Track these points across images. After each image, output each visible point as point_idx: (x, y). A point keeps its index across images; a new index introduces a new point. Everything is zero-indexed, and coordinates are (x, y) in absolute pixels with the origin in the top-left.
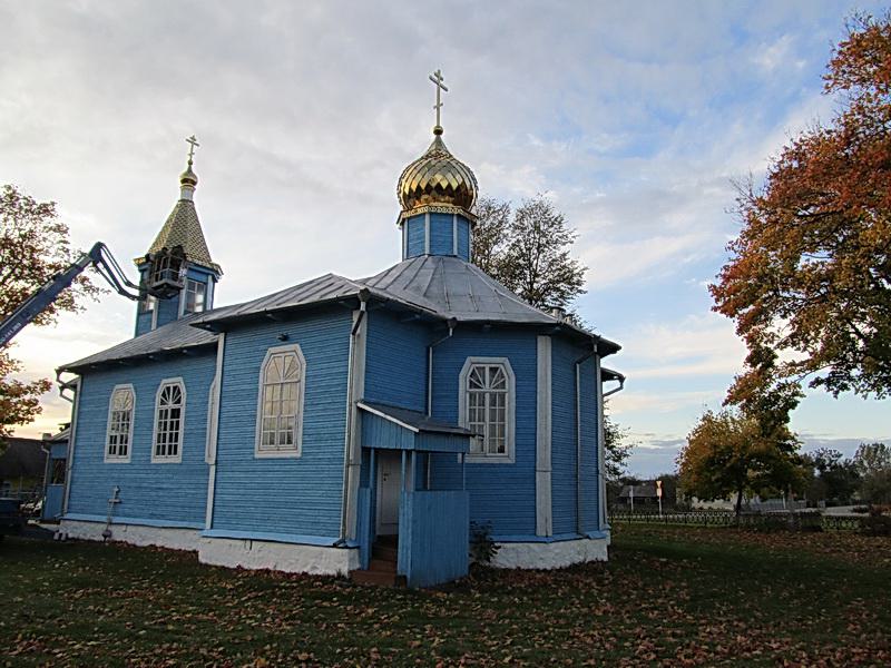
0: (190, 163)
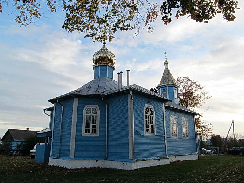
0: (166, 59)
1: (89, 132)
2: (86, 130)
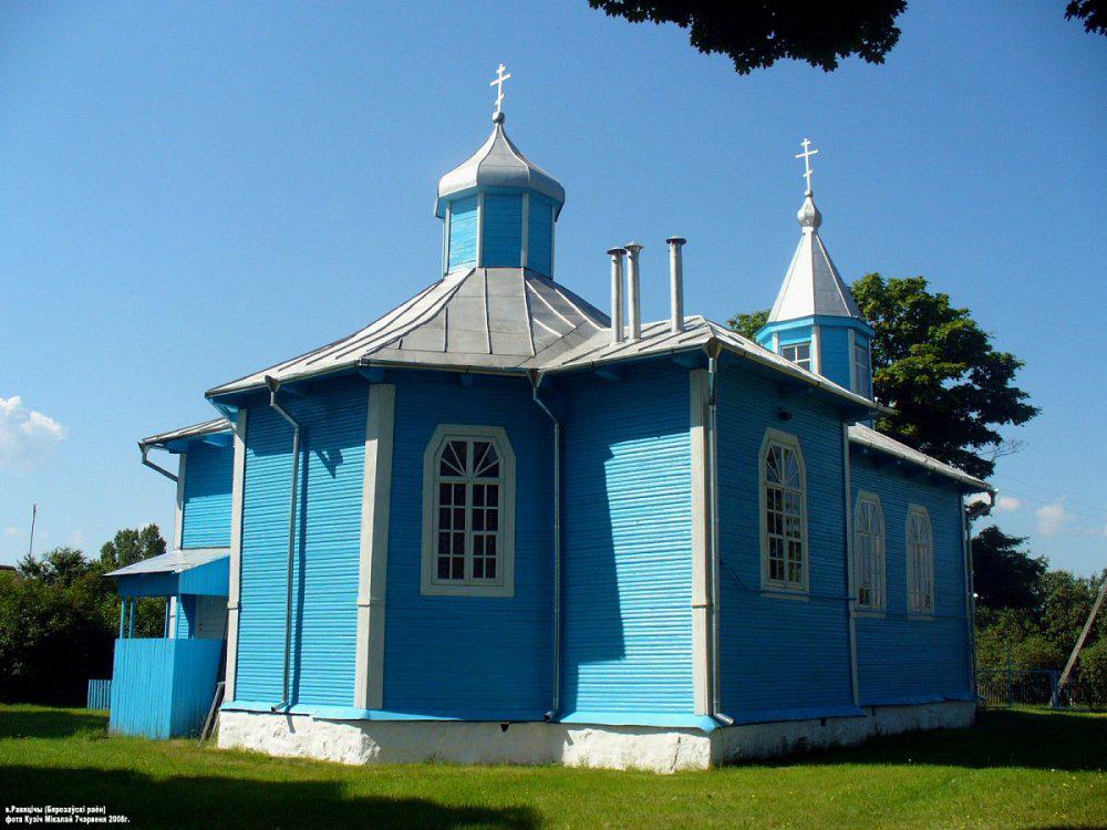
1: (459, 574)
2: (443, 563)
